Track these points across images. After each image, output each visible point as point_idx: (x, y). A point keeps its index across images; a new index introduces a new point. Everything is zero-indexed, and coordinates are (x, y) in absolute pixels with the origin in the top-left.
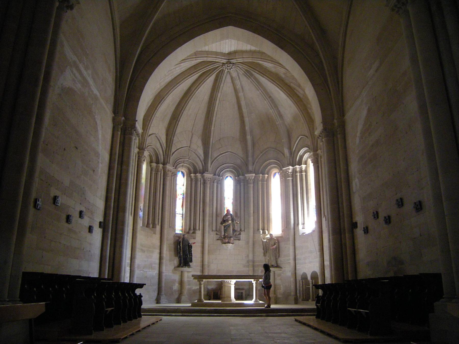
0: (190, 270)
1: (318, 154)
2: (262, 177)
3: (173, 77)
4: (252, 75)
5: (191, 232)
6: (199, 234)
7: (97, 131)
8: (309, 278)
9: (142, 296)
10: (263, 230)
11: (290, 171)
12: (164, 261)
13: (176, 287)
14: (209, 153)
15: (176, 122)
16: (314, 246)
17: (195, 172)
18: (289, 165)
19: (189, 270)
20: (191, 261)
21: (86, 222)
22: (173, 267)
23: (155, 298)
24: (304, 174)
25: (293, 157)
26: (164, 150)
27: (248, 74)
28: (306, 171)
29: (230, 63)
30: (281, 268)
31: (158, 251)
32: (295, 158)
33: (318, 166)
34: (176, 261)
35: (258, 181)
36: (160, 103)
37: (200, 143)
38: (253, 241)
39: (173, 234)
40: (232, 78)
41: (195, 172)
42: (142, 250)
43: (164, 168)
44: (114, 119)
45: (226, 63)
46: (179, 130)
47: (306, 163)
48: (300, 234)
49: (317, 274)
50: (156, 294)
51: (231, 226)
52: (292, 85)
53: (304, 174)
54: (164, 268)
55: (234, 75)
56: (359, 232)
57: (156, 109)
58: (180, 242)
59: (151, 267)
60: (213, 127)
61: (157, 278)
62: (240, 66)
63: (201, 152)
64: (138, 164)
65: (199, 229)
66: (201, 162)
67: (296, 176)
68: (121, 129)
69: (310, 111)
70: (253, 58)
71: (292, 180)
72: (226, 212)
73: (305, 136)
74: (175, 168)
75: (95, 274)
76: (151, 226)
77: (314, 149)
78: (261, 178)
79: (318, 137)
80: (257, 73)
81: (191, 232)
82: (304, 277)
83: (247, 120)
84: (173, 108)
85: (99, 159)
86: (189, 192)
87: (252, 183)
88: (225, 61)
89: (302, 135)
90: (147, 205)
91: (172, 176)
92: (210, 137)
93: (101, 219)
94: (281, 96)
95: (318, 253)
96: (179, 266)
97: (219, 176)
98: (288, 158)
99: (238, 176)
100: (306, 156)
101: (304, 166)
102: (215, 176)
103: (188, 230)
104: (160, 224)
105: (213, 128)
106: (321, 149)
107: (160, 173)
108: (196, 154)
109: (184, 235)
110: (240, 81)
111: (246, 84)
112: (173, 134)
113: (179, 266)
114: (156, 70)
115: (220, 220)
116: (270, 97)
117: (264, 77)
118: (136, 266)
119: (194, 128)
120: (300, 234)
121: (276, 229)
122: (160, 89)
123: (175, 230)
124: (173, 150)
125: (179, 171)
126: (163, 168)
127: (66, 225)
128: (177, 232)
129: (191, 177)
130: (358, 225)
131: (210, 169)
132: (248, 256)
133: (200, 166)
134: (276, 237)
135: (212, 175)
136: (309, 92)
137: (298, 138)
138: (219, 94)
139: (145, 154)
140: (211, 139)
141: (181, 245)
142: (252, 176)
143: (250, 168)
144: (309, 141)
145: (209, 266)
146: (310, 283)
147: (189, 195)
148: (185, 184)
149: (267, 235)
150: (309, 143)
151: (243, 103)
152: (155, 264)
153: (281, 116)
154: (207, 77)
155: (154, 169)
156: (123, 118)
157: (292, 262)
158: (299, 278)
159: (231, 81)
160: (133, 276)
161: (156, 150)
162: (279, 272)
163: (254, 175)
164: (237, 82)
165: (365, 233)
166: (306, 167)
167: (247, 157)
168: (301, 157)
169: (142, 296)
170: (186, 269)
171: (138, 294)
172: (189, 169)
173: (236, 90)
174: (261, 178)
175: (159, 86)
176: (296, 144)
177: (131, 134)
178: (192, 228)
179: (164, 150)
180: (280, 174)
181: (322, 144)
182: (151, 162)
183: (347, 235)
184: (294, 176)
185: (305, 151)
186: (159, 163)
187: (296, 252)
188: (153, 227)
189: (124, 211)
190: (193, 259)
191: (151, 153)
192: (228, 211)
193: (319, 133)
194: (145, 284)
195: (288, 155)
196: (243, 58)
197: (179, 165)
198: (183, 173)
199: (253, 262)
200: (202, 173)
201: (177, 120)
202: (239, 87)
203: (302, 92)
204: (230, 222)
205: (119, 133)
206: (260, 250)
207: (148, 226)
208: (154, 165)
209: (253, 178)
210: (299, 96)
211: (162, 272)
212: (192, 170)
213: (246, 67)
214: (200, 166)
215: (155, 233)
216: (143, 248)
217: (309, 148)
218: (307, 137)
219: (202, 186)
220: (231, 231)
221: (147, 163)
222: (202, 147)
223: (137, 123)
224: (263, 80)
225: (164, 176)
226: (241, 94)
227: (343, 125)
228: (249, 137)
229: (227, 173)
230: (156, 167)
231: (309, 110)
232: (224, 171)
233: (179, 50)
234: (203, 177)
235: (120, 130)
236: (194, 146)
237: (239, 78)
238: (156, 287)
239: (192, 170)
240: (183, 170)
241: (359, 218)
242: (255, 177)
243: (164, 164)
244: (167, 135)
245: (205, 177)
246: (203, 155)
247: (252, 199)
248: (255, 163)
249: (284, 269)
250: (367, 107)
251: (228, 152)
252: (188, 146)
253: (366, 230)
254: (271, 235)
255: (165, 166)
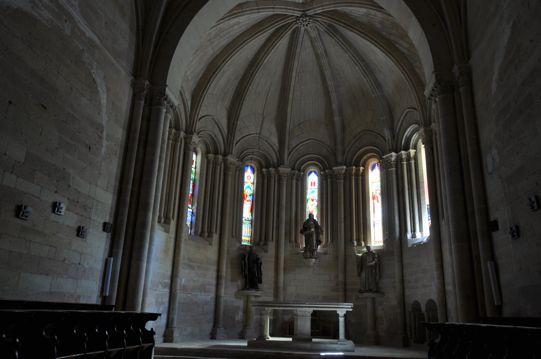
0: (259, 294)
1: (431, 131)
2: (356, 170)
3: (231, 39)
4: (337, 31)
5: (262, 243)
6: (272, 246)
7: (94, 91)
8: (423, 309)
9: (154, 333)
10: (359, 240)
11: (393, 159)
12: (223, 281)
13: (239, 316)
14: (285, 140)
15: (240, 101)
16: (429, 262)
17: (268, 167)
18: (390, 151)
19: (258, 293)
20: (260, 282)
21: (68, 218)
22: (235, 290)
23: (209, 332)
24: (413, 162)
25: (397, 141)
26: (225, 137)
27: (332, 31)
28: (416, 158)
29: (306, 16)
30: (384, 294)
31: (215, 268)
32: (399, 141)
33: (432, 148)
34: (240, 283)
35: (351, 175)
36: (214, 73)
37: (274, 129)
38: (345, 256)
39: (238, 245)
40: (310, 38)
41: (268, 167)
42: (189, 266)
43: (225, 161)
44: (134, 85)
45: (301, 17)
46: (244, 112)
47: (415, 147)
48: (409, 246)
49: (435, 303)
50: (210, 326)
51: (314, 236)
52: (392, 37)
53: (413, 162)
54: (223, 290)
55: (314, 34)
56: (501, 238)
57: (209, 81)
58: (245, 256)
59: (203, 288)
60: (289, 106)
61: (213, 303)
62: (319, 19)
63: (275, 140)
64: (185, 153)
65: (272, 240)
66: (276, 153)
67: (402, 165)
68: (146, 99)
69: (418, 71)
70: (335, 4)
71: (397, 171)
72: (307, 217)
73: (412, 108)
74: (242, 161)
75: (94, 299)
76: (206, 234)
77: (426, 124)
78: (354, 171)
79: (429, 98)
80: (343, 27)
81: (262, 243)
82: (416, 305)
83: (333, 95)
84: (236, 83)
85: (102, 132)
86: (260, 192)
87: (342, 178)
88: (298, 14)
89: (408, 108)
90: (202, 207)
91: (236, 171)
92: (286, 121)
93: (107, 218)
94: (377, 56)
95: (435, 274)
96: (245, 288)
97: (299, 171)
98: (390, 141)
99: (324, 170)
100: (415, 136)
101: (412, 152)
102: (293, 171)
103: (258, 240)
104: (218, 233)
105: (289, 109)
106: (435, 122)
107: (219, 167)
108: (269, 144)
109: (251, 247)
110: (322, 42)
111: (331, 45)
112: (237, 117)
113: (245, 288)
114: (196, 18)
115: (300, 228)
116: (363, 61)
117: (351, 31)
118: (178, 287)
119: (265, 110)
120: (409, 246)
121: (376, 238)
122: (215, 56)
123: (240, 240)
124: (238, 136)
125: (247, 166)
126: (185, 138)
127: (18, 221)
128: (244, 243)
129: (262, 172)
130: (500, 225)
131: (286, 161)
132: (337, 276)
133: (274, 159)
134: (375, 250)
135: (290, 169)
136: (416, 34)
137: (403, 112)
138: (296, 63)
139: (193, 140)
140: (288, 123)
141: (246, 261)
142: (343, 169)
143: (340, 158)
144: (417, 115)
145: (285, 289)
146: (426, 316)
147: (260, 196)
148: (255, 182)
149: (363, 248)
150: (419, 119)
151: (327, 73)
152: (210, 285)
153: (378, 85)
154: (277, 38)
155: (212, 162)
156: (147, 82)
157: (398, 285)
158: (409, 309)
159: (310, 45)
160: (174, 301)
161: (215, 138)
162: (380, 299)
163: (345, 167)
164: (318, 44)
165: (513, 236)
166: (416, 153)
167: (336, 145)
168: (409, 139)
169: (154, 333)
170: (253, 292)
171: (149, 329)
172: (260, 163)
173: (318, 57)
174: (354, 171)
175: (212, 52)
176: (400, 122)
177: (160, 104)
178: (263, 239)
179: (225, 137)
180: (380, 165)
181: (435, 109)
182: (208, 152)
183: (480, 242)
184: (399, 166)
185: (413, 131)
186: (218, 154)
187: (405, 271)
188: (209, 236)
189: (146, 208)
190: (264, 279)
191: (208, 141)
192: (311, 215)
193: (433, 85)
194: (160, 315)
195: (390, 138)
196: (323, 6)
197: (246, 157)
198: (252, 168)
199: (345, 284)
200: (276, 167)
201: (241, 99)
202: (320, 51)
203: (406, 45)
204: (313, 230)
205: (142, 103)
206: (353, 268)
207: (202, 235)
208: (211, 156)
209: (344, 171)
210: (402, 53)
211: (220, 297)
212: (264, 163)
213: (327, 21)
214: (274, 159)
215: (210, 244)
216: (191, 263)
217: (419, 124)
218: (416, 109)
219: (276, 183)
220: (315, 242)
221: (202, 154)
222: (276, 135)
223: (167, 89)
224: (352, 35)
225: (225, 170)
226: (324, 61)
227: (468, 73)
228: (337, 119)
229: (310, 167)
230: (215, 159)
231: (416, 69)
232: (305, 164)
233: (379, 184)
234: (277, 172)
235: (143, 99)
236: (265, 133)
237: (321, 39)
238: (211, 316)
239: (264, 163)
240: (252, 165)
241: (500, 214)
242: (346, 170)
243: (225, 155)
244: (229, 118)
245: (281, 172)
246: (277, 145)
247: (343, 198)
248: (346, 152)
249: (387, 294)
250: (511, 24)
251: (310, 139)
252: (258, 132)
253: (516, 232)
254: (368, 248)
255: (226, 158)
